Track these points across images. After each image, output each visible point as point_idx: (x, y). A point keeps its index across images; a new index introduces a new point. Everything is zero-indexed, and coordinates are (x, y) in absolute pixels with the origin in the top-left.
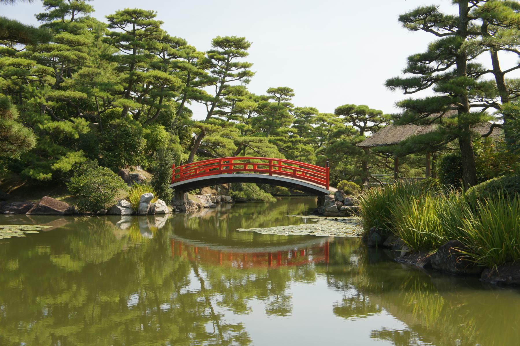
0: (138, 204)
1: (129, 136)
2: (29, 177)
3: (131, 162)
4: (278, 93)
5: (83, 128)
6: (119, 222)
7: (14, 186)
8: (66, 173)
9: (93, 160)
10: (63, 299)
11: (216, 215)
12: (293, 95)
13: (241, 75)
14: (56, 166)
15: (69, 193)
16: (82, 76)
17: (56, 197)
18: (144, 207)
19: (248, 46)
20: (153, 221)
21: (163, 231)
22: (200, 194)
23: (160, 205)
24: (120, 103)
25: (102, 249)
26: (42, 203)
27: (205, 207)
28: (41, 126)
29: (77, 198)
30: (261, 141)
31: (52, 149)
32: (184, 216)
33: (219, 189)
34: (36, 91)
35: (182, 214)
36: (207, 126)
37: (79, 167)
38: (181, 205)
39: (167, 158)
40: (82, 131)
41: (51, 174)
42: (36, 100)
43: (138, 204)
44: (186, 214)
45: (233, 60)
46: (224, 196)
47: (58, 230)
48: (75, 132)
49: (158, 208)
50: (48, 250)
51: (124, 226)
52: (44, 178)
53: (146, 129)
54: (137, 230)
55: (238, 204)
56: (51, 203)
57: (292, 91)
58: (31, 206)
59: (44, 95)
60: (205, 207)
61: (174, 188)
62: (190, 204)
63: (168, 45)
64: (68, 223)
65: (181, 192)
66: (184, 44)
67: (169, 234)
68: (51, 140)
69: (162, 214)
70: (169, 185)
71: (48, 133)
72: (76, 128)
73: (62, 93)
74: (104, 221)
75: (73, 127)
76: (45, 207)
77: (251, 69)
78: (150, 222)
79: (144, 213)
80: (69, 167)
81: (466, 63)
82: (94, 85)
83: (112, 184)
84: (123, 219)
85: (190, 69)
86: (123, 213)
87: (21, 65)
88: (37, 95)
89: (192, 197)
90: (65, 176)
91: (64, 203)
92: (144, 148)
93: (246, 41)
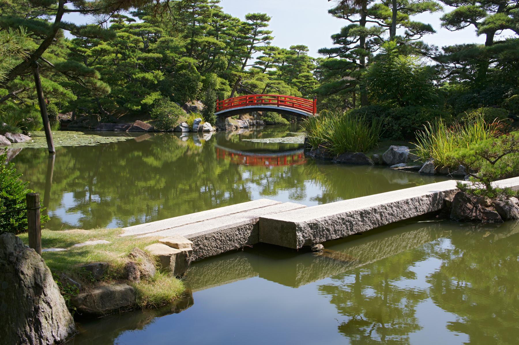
0: (192, 125)
1: (191, 81)
2: (128, 109)
3: (192, 98)
4: (298, 49)
5: (160, 77)
6: (181, 136)
7: (121, 114)
8: (149, 106)
9: (167, 97)
10: (152, 183)
11: (254, 133)
12: (308, 50)
13: (265, 39)
14: (144, 101)
15: (152, 118)
16: (163, 42)
17: (145, 121)
18: (197, 127)
19: (269, 19)
20: (202, 136)
21: (210, 142)
22: (239, 119)
23: (207, 126)
24: (183, 60)
25: (171, 154)
26: (135, 125)
27: (241, 128)
28: (134, 76)
29: (155, 121)
30: (279, 84)
31: (141, 90)
32: (225, 134)
33: (255, 116)
34: (131, 54)
35: (224, 131)
36: (240, 74)
37: (158, 102)
38: (223, 126)
39: (212, 96)
40: (159, 79)
41: (140, 107)
42: (131, 60)
43: (192, 125)
44: (227, 132)
45: (259, 29)
46: (258, 121)
47: (145, 141)
48: (155, 80)
49: (205, 127)
50: (141, 154)
51: (184, 139)
52: (137, 109)
53: (203, 76)
54: (191, 142)
55: (268, 126)
56: (141, 124)
57: (306, 47)
58: (129, 127)
59: (136, 57)
60: (241, 128)
61: (217, 115)
62: (230, 125)
63: (219, 19)
64: (150, 137)
65: (223, 117)
66: (230, 17)
67: (215, 144)
68: (141, 85)
69: (208, 131)
70: (214, 113)
71: (139, 81)
72: (155, 77)
73: (147, 55)
74: (172, 136)
75: (154, 77)
76: (137, 127)
77: (271, 35)
78: (200, 136)
79: (196, 131)
80: (151, 102)
81: (163, 80)
82: (168, 48)
83: (176, 113)
84: (183, 134)
85: (234, 35)
86: (183, 131)
87: (124, 37)
88: (131, 57)
89: (233, 121)
90: (150, 108)
91: (149, 125)
92: (201, 89)
93: (267, 16)
